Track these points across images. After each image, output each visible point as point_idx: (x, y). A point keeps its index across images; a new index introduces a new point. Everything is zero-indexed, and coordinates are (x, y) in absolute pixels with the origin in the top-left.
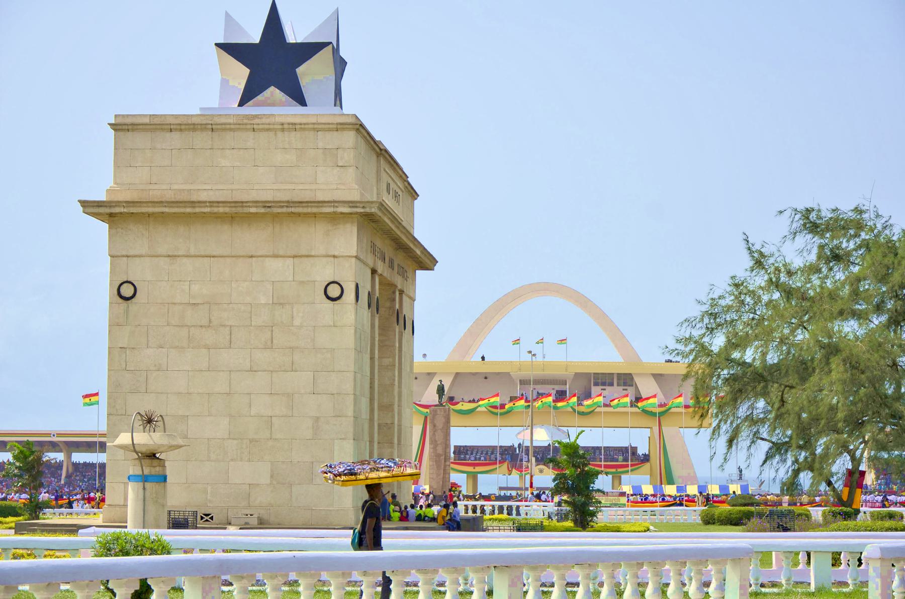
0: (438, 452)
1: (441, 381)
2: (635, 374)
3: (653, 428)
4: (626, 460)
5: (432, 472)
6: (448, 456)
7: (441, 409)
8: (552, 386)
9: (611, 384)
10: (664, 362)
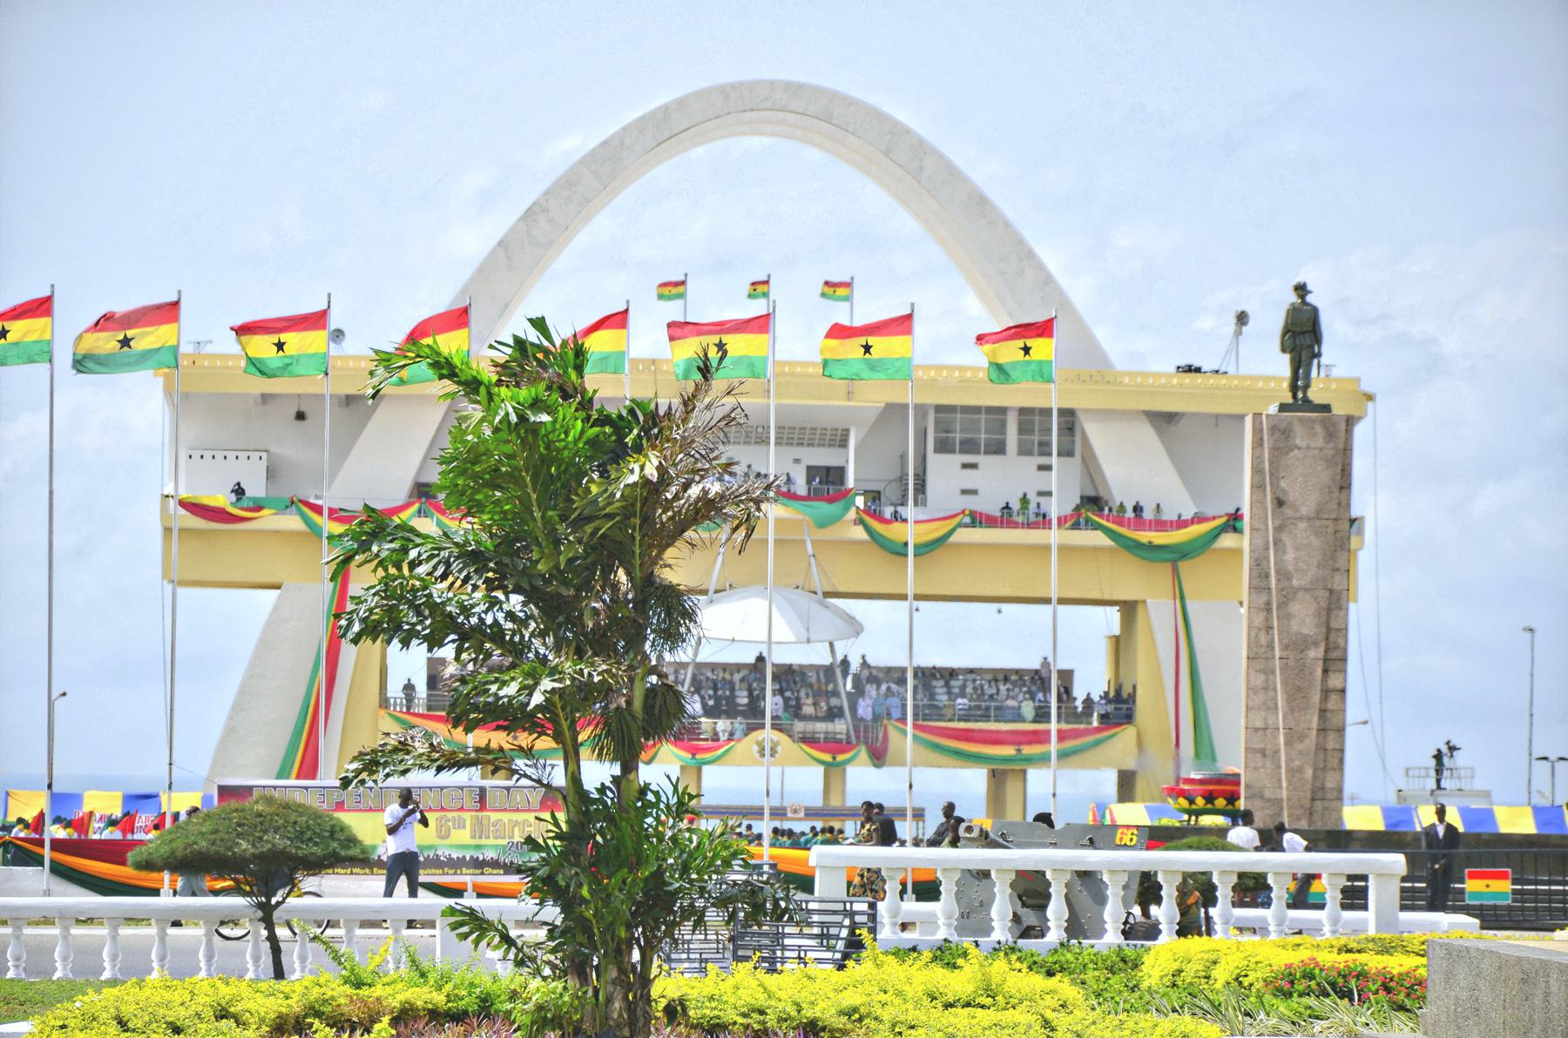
0: (1295, 627)
1: (1301, 289)
2: (1087, 411)
3: (1149, 601)
4: (1042, 715)
5: (1259, 723)
6: (1336, 648)
7: (1314, 421)
9: (998, 448)
10: (1173, 370)
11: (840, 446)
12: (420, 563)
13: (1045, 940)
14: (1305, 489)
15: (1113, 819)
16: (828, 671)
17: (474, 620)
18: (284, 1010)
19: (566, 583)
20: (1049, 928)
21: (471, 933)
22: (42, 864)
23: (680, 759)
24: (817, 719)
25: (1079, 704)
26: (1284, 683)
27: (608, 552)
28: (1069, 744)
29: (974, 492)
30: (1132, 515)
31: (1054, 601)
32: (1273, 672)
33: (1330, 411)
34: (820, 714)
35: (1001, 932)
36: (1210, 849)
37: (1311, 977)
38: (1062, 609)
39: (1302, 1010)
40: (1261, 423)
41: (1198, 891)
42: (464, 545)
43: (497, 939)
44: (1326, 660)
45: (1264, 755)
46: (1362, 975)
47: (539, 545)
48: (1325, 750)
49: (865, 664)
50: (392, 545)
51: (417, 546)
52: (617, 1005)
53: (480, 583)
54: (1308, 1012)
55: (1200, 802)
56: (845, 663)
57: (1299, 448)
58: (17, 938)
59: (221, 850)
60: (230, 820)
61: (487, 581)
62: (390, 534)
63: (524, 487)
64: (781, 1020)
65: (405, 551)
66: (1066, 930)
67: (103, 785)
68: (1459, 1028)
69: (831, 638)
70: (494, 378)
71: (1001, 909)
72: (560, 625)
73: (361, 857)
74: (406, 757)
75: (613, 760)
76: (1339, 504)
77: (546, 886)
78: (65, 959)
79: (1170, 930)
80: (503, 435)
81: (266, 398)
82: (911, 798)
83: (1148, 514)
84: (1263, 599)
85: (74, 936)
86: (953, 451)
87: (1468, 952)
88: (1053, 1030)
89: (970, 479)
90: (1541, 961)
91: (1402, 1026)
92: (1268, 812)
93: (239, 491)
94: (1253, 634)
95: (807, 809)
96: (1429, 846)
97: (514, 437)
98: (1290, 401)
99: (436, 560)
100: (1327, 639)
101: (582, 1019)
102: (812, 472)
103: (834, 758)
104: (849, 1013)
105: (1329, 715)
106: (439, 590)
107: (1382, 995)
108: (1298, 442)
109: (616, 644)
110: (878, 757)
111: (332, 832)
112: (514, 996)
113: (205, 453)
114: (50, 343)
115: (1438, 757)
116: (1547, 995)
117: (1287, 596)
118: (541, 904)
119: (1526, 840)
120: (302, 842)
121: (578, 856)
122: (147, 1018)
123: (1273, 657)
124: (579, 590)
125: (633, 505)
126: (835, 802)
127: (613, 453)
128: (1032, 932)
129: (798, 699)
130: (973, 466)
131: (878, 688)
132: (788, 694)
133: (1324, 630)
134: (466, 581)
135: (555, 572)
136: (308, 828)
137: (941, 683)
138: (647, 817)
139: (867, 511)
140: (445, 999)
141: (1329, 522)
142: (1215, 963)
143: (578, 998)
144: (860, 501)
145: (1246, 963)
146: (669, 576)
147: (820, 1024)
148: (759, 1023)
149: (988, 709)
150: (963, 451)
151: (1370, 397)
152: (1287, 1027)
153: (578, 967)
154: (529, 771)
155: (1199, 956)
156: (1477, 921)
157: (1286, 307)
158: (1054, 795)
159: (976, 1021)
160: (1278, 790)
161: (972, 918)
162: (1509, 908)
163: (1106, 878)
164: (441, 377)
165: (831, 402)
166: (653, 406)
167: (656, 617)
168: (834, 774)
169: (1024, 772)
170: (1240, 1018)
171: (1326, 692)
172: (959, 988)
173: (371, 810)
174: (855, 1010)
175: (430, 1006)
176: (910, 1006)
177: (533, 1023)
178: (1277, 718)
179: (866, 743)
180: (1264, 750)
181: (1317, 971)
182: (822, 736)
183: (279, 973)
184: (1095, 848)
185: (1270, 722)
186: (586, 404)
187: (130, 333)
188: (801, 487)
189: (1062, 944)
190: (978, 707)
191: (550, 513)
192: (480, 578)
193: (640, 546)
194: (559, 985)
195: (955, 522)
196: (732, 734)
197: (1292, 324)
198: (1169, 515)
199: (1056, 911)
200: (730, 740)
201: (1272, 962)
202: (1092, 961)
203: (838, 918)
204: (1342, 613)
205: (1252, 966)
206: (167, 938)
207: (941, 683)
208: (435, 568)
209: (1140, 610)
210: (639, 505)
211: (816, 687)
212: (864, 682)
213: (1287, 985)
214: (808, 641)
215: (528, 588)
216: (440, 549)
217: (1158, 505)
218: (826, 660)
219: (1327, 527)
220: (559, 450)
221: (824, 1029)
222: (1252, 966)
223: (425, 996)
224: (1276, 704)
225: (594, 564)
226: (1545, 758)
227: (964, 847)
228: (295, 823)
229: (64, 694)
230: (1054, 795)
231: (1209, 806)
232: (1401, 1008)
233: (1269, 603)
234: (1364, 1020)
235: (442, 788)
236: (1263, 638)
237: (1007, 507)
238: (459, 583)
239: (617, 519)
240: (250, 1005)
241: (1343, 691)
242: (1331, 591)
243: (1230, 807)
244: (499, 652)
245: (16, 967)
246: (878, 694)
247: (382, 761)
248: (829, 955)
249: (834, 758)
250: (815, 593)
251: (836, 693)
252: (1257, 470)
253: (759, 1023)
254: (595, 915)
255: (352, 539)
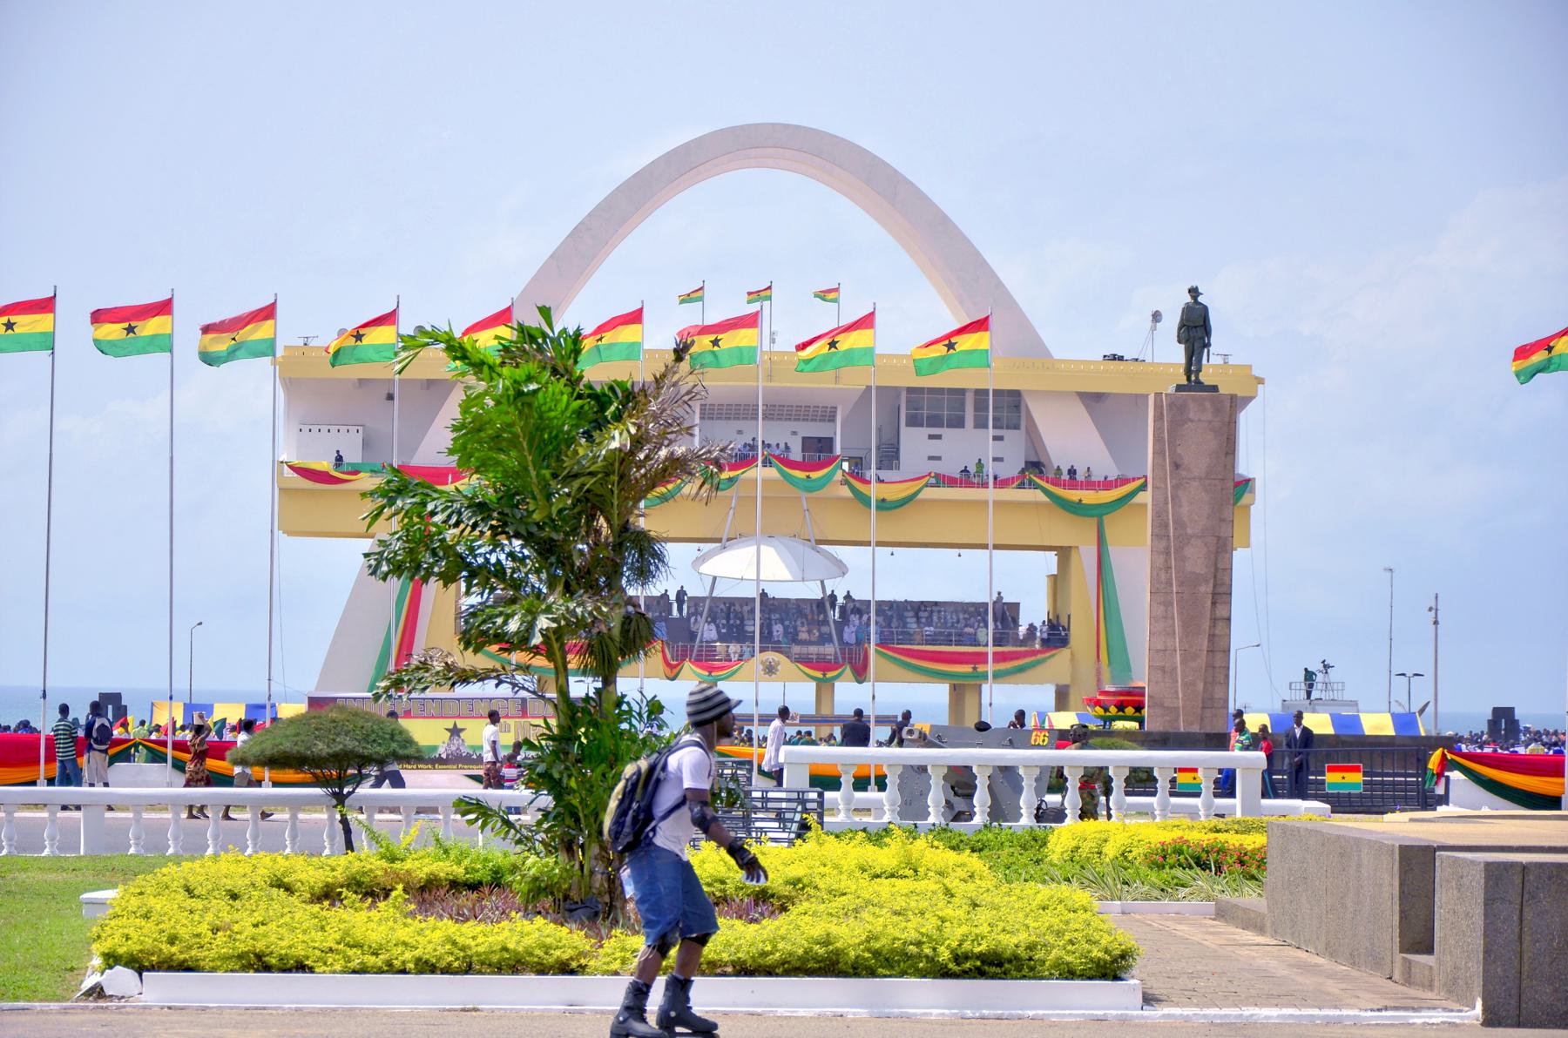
1: (1194, 292)
2: (1031, 392)
5: (1160, 646)
6: (1222, 584)
8: (794, 425)
9: (958, 423)
11: (829, 421)
12: (437, 513)
13: (972, 822)
14: (1197, 450)
15: (1051, 724)
16: (819, 605)
17: (480, 560)
18: (330, 880)
19: (555, 528)
20: (975, 813)
21: (477, 819)
22: (166, 762)
23: (699, 675)
24: (809, 643)
25: (1022, 630)
26: (1180, 613)
27: (590, 504)
28: (1002, 666)
29: (939, 458)
30: (1067, 477)
31: (991, 546)
32: (1172, 604)
33: (1218, 391)
34: (813, 639)
35: (934, 818)
36: (1111, 749)
37: (1180, 852)
38: (878, 549)
39: (1170, 879)
40: (1162, 400)
41: (1095, 783)
42: (472, 498)
43: (499, 824)
44: (1214, 594)
45: (1164, 672)
46: (1222, 851)
47: (534, 498)
48: (1214, 667)
49: (848, 597)
50: (414, 500)
51: (434, 499)
52: (599, 876)
53: (485, 529)
54: (1175, 881)
55: (1113, 710)
56: (833, 597)
57: (1192, 421)
58: (10, 822)
59: (302, 749)
60: (309, 725)
61: (492, 527)
62: (411, 491)
63: (521, 450)
64: (738, 889)
65: (424, 504)
66: (989, 814)
67: (228, 698)
68: (1291, 894)
69: (822, 578)
70: (498, 361)
71: (935, 799)
72: (552, 564)
73: (417, 755)
74: (426, 675)
75: (595, 675)
76: (1225, 466)
77: (542, 780)
78: (176, 839)
79: (1073, 814)
80: (504, 407)
81: (362, 382)
82: (873, 708)
83: (1080, 477)
84: (1163, 544)
85: (302, 821)
86: (922, 426)
87: (1299, 832)
88: (952, 896)
89: (935, 447)
90: (1355, 838)
91: (1251, 892)
92: (1167, 718)
93: (339, 459)
94: (1155, 574)
95: (802, 716)
96: (1289, 745)
97: (512, 409)
98: (1186, 383)
99: (450, 510)
100: (1215, 577)
101: (570, 888)
102: (807, 443)
103: (824, 675)
104: (795, 882)
105: (1217, 639)
106: (451, 534)
107: (1237, 867)
108: (1191, 415)
109: (597, 580)
110: (860, 673)
111: (392, 736)
112: (514, 869)
113: (341, 428)
114: (171, 336)
115: (1309, 675)
116: (1359, 865)
117: (1183, 540)
118: (536, 793)
119: (1378, 742)
120: (368, 743)
121: (566, 754)
122: (210, 887)
123: (1172, 592)
124: (567, 534)
125: (612, 464)
126: (825, 711)
127: (597, 424)
128: (962, 817)
129: (795, 628)
130: (938, 437)
131: (860, 618)
132: (787, 623)
133: (1213, 570)
134: (474, 526)
135: (547, 521)
136: (373, 731)
137: (911, 614)
138: (621, 722)
139: (851, 474)
140: (463, 871)
141: (1217, 481)
142: (1106, 841)
143: (566, 870)
144: (846, 466)
145: (1130, 841)
146: (642, 523)
147: (770, 891)
148: (720, 891)
149: (950, 634)
150: (929, 425)
151: (1261, 381)
152: (1156, 893)
153: (569, 847)
154: (527, 685)
155: (1093, 836)
156: (1329, 806)
157: (1182, 305)
158: (991, 705)
159: (896, 889)
160: (1175, 700)
161: (912, 806)
162: (1360, 796)
163: (1021, 772)
164: (455, 358)
165: (818, 385)
166: (629, 385)
167: (631, 557)
168: (824, 690)
169: (981, 685)
170: (1119, 886)
171: (1214, 621)
172: (885, 862)
173: (433, 717)
174: (799, 880)
175: (451, 877)
176: (844, 877)
177: (529, 891)
178: (1175, 642)
179: (850, 663)
180: (1164, 667)
181: (1185, 848)
182: (814, 657)
183: (349, 846)
184: (1014, 748)
185: (1169, 644)
186: (573, 382)
187: (133, 324)
188: (796, 454)
189: (985, 826)
190: (941, 634)
191: (544, 472)
192: (486, 525)
193: (618, 498)
194: (551, 860)
195: (923, 481)
196: (741, 656)
197: (1187, 320)
198: (1097, 476)
199: (981, 799)
200: (740, 660)
201: (1152, 841)
202: (1008, 840)
203: (793, 805)
204: (1227, 556)
205: (1135, 844)
206: (298, 823)
207: (911, 614)
208: (449, 517)
209: (1073, 552)
210: (617, 464)
211: (809, 617)
212: (849, 612)
213: (1161, 858)
214: (803, 580)
215: (525, 534)
216: (452, 501)
217: (1089, 468)
218: (818, 595)
219: (1215, 485)
220: (550, 419)
221: (773, 896)
222: (1135, 844)
223: (446, 868)
224: (1174, 631)
225: (580, 514)
226: (1403, 675)
227: (908, 746)
228: (362, 727)
229: (200, 624)
230: (991, 705)
231: (1121, 713)
232: (1253, 877)
233: (1167, 548)
234: (1220, 887)
235: (491, 699)
236: (1163, 577)
237: (965, 470)
238: (469, 529)
239: (600, 476)
240: (303, 876)
241: (1229, 619)
242: (1219, 538)
243: (1137, 714)
244: (502, 586)
245: (137, 844)
246: (861, 623)
247: (406, 679)
248: (785, 835)
249: (824, 675)
250: (809, 540)
251: (826, 622)
252: (1158, 439)
253: (720, 891)
254: (581, 803)
255: (380, 496)
